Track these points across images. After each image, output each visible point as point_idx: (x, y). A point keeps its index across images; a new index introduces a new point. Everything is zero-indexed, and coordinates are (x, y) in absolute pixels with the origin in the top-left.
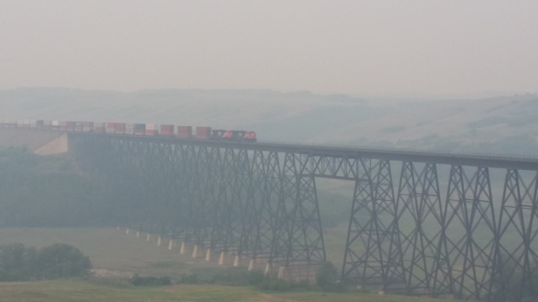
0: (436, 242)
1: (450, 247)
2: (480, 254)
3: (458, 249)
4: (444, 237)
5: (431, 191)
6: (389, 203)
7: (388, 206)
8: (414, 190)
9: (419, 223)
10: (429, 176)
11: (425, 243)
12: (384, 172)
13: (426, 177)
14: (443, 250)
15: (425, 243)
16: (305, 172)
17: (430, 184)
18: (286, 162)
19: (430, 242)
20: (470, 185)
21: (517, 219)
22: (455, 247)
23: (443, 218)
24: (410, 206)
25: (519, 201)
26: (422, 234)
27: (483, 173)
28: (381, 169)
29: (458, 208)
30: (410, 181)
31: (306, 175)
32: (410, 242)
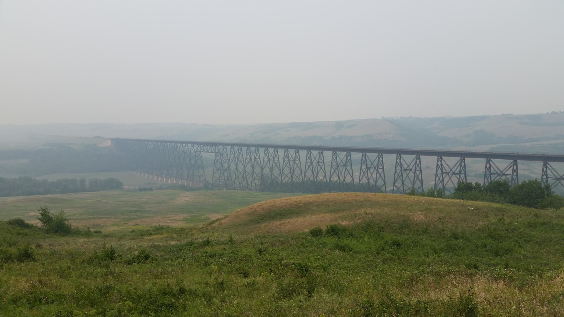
0: (242, 173)
5: (240, 156)
9: (237, 167)
21: (268, 164)
25: (269, 158)
28: (379, 159)
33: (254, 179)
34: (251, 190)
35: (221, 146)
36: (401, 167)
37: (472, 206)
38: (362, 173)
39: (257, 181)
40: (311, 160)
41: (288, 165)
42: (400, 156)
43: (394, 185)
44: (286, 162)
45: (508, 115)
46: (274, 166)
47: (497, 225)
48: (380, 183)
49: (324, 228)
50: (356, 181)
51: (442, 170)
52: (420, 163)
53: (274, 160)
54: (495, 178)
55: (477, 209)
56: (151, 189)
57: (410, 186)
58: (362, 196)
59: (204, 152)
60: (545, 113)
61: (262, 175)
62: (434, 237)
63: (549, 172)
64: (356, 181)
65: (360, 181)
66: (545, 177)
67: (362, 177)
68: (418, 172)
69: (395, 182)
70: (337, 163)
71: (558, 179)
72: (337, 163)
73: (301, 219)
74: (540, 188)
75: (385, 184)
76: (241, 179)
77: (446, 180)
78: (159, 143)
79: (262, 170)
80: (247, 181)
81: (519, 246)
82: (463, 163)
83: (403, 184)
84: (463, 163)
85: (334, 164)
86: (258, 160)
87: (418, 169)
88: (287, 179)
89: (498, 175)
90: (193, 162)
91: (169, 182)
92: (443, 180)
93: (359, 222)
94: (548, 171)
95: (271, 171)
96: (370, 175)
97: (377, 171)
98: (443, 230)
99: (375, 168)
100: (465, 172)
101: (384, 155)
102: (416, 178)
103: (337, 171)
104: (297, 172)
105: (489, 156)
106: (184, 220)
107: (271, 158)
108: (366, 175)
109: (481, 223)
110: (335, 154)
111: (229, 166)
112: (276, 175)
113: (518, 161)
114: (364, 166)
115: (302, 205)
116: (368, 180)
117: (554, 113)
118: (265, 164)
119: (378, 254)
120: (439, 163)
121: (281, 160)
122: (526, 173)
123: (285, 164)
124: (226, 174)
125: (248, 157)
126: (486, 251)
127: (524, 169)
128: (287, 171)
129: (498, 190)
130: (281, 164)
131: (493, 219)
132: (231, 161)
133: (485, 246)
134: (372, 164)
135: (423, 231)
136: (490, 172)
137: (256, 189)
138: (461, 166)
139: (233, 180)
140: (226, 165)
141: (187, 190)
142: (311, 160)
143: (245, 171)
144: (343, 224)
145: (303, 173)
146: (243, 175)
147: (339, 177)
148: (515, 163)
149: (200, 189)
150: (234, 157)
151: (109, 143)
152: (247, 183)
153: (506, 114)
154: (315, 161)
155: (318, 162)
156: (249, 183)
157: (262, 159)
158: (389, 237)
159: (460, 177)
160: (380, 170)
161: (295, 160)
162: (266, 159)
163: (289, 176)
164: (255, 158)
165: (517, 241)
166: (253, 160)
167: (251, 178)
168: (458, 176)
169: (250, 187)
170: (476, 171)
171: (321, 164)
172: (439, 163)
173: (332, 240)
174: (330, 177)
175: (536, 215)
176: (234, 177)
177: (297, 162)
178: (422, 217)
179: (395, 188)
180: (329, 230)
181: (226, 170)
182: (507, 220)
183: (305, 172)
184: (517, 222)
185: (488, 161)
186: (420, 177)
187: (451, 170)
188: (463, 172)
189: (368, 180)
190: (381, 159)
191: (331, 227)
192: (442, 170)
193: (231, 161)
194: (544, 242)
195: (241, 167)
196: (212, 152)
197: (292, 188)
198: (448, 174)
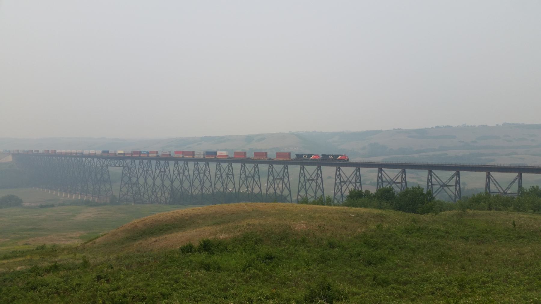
0: (152, 186)
1: (156, 187)
5: (150, 169)
9: (146, 180)
21: (178, 177)
25: (179, 171)
26: (147, 184)
28: (255, 168)
33: (164, 192)
34: (160, 203)
35: (130, 160)
36: (304, 178)
37: (353, 213)
38: (269, 184)
39: (167, 195)
40: (220, 172)
41: (198, 177)
42: (303, 167)
43: (298, 194)
44: (219, 176)
45: (398, 129)
46: (184, 180)
47: (375, 231)
48: (286, 192)
49: (196, 244)
50: (264, 191)
51: (340, 179)
52: (321, 173)
53: (184, 173)
54: (386, 186)
55: (358, 215)
56: (53, 206)
57: (313, 195)
58: (243, 206)
59: (111, 166)
60: (430, 127)
61: (172, 188)
62: (310, 247)
63: (433, 180)
64: (264, 191)
65: (267, 191)
66: (430, 184)
67: (270, 187)
68: (319, 182)
69: (299, 192)
70: (245, 175)
71: (441, 186)
72: (245, 175)
73: (180, 234)
74: (422, 194)
75: (290, 194)
76: (150, 193)
77: (344, 189)
78: (63, 158)
79: (172, 183)
80: (157, 194)
81: (394, 253)
82: (358, 173)
83: (306, 193)
84: (358, 173)
85: (243, 175)
86: (168, 173)
87: (319, 179)
88: (197, 191)
89: (389, 183)
90: (99, 176)
91: (74, 198)
92: (341, 189)
93: (238, 234)
94: (433, 179)
95: (181, 183)
96: (276, 186)
97: (283, 181)
98: (321, 239)
99: (281, 179)
100: (360, 180)
101: (289, 166)
102: (317, 187)
103: (245, 182)
104: (207, 184)
105: (380, 166)
106: (80, 237)
107: (181, 171)
108: (273, 185)
109: (359, 230)
110: (243, 166)
111: (137, 180)
112: (186, 188)
113: (460, 172)
114: (271, 177)
115: (187, 218)
116: (275, 190)
117: (437, 127)
118: (174, 177)
119: (244, 271)
120: (338, 173)
121: (191, 173)
122: (415, 181)
123: (195, 177)
124: (134, 188)
125: (158, 171)
126: (359, 260)
127: (413, 178)
128: (197, 183)
129: (385, 196)
130: (191, 177)
131: (372, 226)
132: (139, 174)
133: (359, 255)
134: (278, 175)
135: (301, 242)
136: (382, 180)
137: (166, 203)
138: (357, 175)
139: (142, 194)
140: (134, 180)
141: (91, 206)
142: (220, 172)
143: (154, 184)
144: (221, 237)
145: (213, 185)
146: (153, 188)
147: (248, 188)
148: (404, 172)
149: (105, 204)
150: (143, 170)
151: (10, 159)
152: (156, 196)
153: (396, 128)
154: (225, 173)
155: (227, 174)
156: (158, 196)
157: (172, 173)
158: (264, 249)
159: (356, 185)
160: (286, 181)
161: (205, 173)
162: (176, 172)
163: (199, 187)
164: (165, 171)
165: (392, 249)
166: (163, 174)
167: (160, 191)
168: (354, 184)
169: (159, 200)
170: (370, 181)
171: (230, 176)
172: (338, 173)
173: (203, 257)
174: (239, 188)
175: (414, 221)
176: (142, 191)
177: (207, 175)
178: (304, 226)
179: (299, 197)
180: (201, 245)
181: (134, 184)
182: (386, 226)
183: (215, 184)
184: (395, 228)
185: (380, 171)
186: (321, 186)
187: (348, 179)
188: (358, 181)
189: (275, 190)
190: (286, 170)
191: (204, 242)
192: (340, 179)
193: (139, 174)
194: (418, 248)
195: (150, 181)
196: (119, 166)
197: (202, 199)
198: (345, 183)
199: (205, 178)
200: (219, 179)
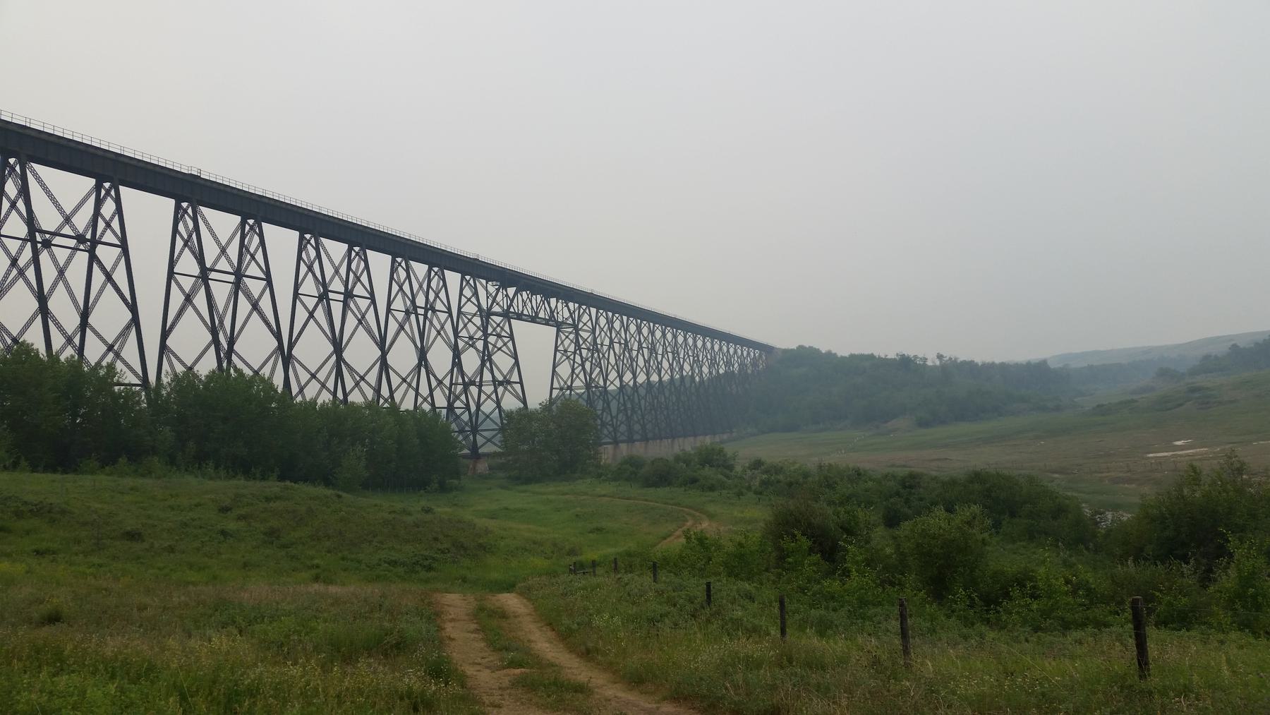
0: (372, 378)
1: (395, 381)
2: (357, 384)
3: (319, 381)
4: (384, 366)
5: (359, 290)
6: (506, 340)
7: (505, 344)
8: (413, 302)
9: (422, 354)
10: (434, 284)
11: (434, 383)
12: (108, 208)
13: (429, 286)
14: (385, 392)
15: (434, 383)
16: (496, 309)
17: (437, 296)
18: (462, 289)
19: (440, 382)
20: (108, 225)
21: (320, 314)
22: (313, 376)
23: (383, 339)
24: (407, 327)
25: (323, 284)
26: (429, 372)
27: (357, 254)
28: (99, 203)
29: (194, 290)
30: (406, 287)
31: (496, 314)
32: (410, 385)
37: (236, 370)
40: (200, 259)
41: (200, 300)
44: (187, 283)
132: (393, 327)
142: (200, 259)
161: (239, 274)
162: (309, 287)
171: (255, 287)
183: (165, 334)
186: (120, 277)
193: (393, 327)
195: (361, 353)
199: (244, 306)
200: (188, 299)
